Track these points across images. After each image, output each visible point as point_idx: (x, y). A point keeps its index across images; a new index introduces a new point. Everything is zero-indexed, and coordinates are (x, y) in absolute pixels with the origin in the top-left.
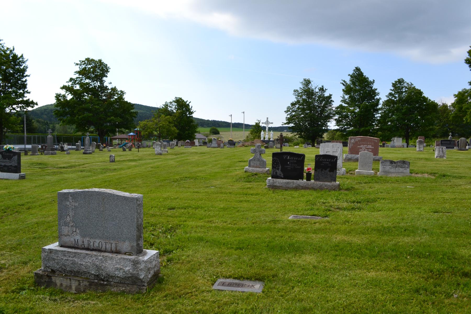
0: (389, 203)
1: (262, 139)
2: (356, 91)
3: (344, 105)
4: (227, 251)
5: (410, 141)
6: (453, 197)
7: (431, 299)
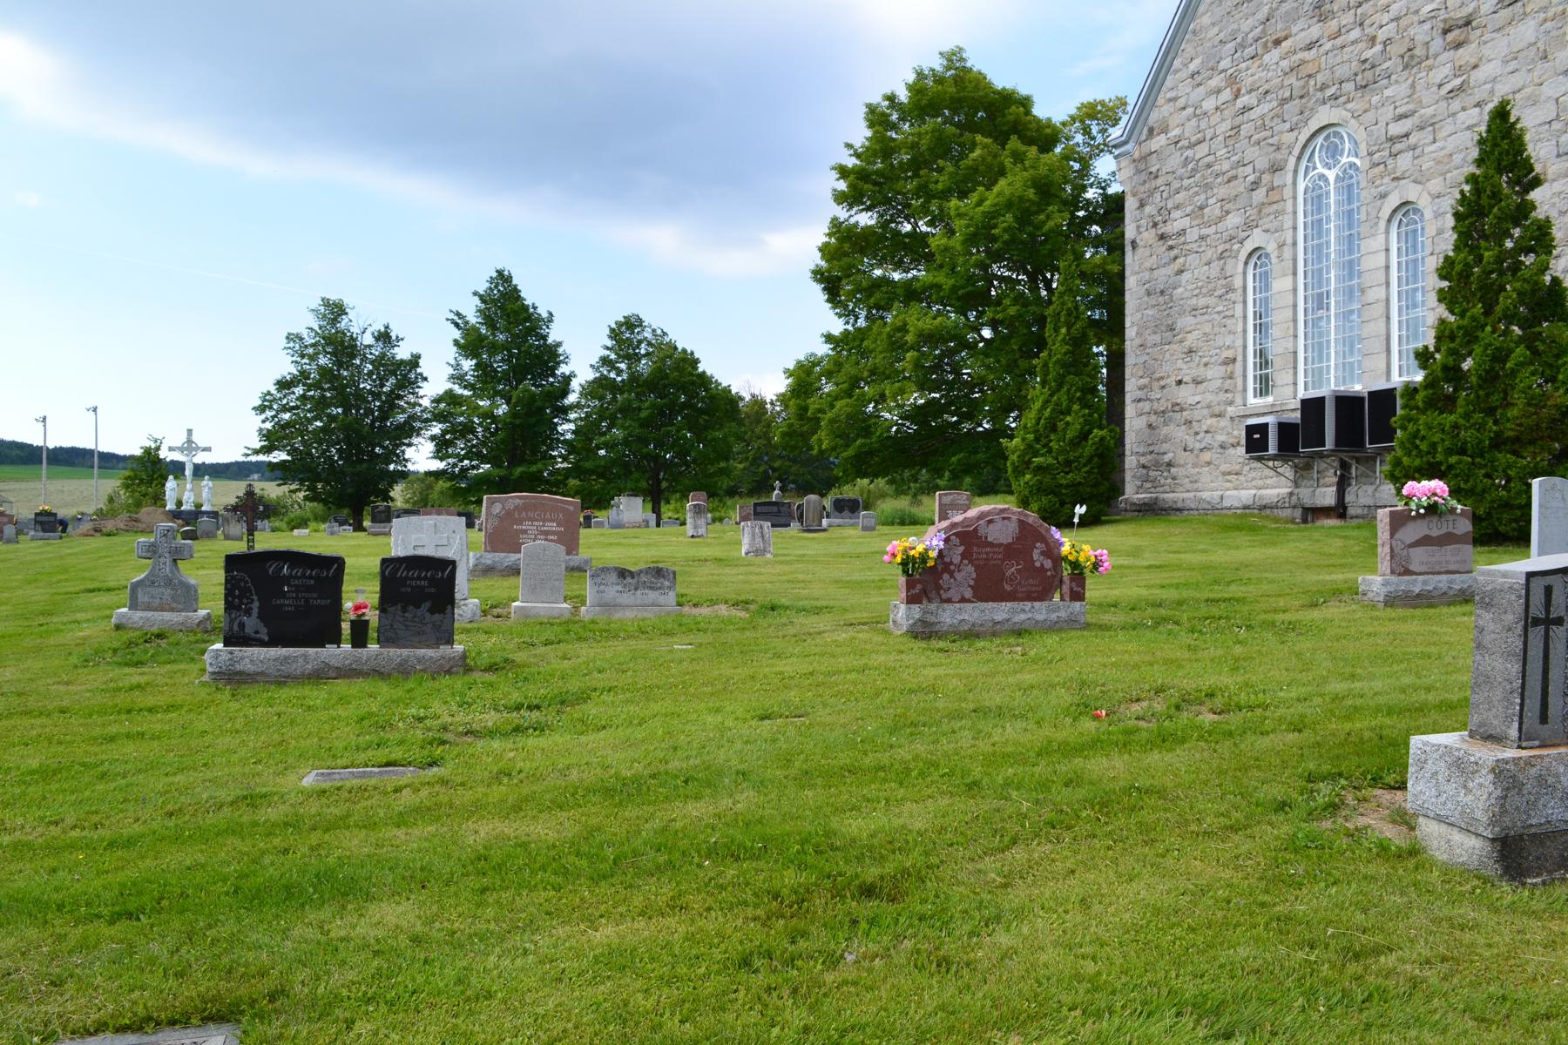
0: (627, 701)
1: (170, 506)
2: (494, 348)
3: (458, 390)
4: (76, 934)
5: (664, 508)
6: (805, 668)
7: (786, 981)
